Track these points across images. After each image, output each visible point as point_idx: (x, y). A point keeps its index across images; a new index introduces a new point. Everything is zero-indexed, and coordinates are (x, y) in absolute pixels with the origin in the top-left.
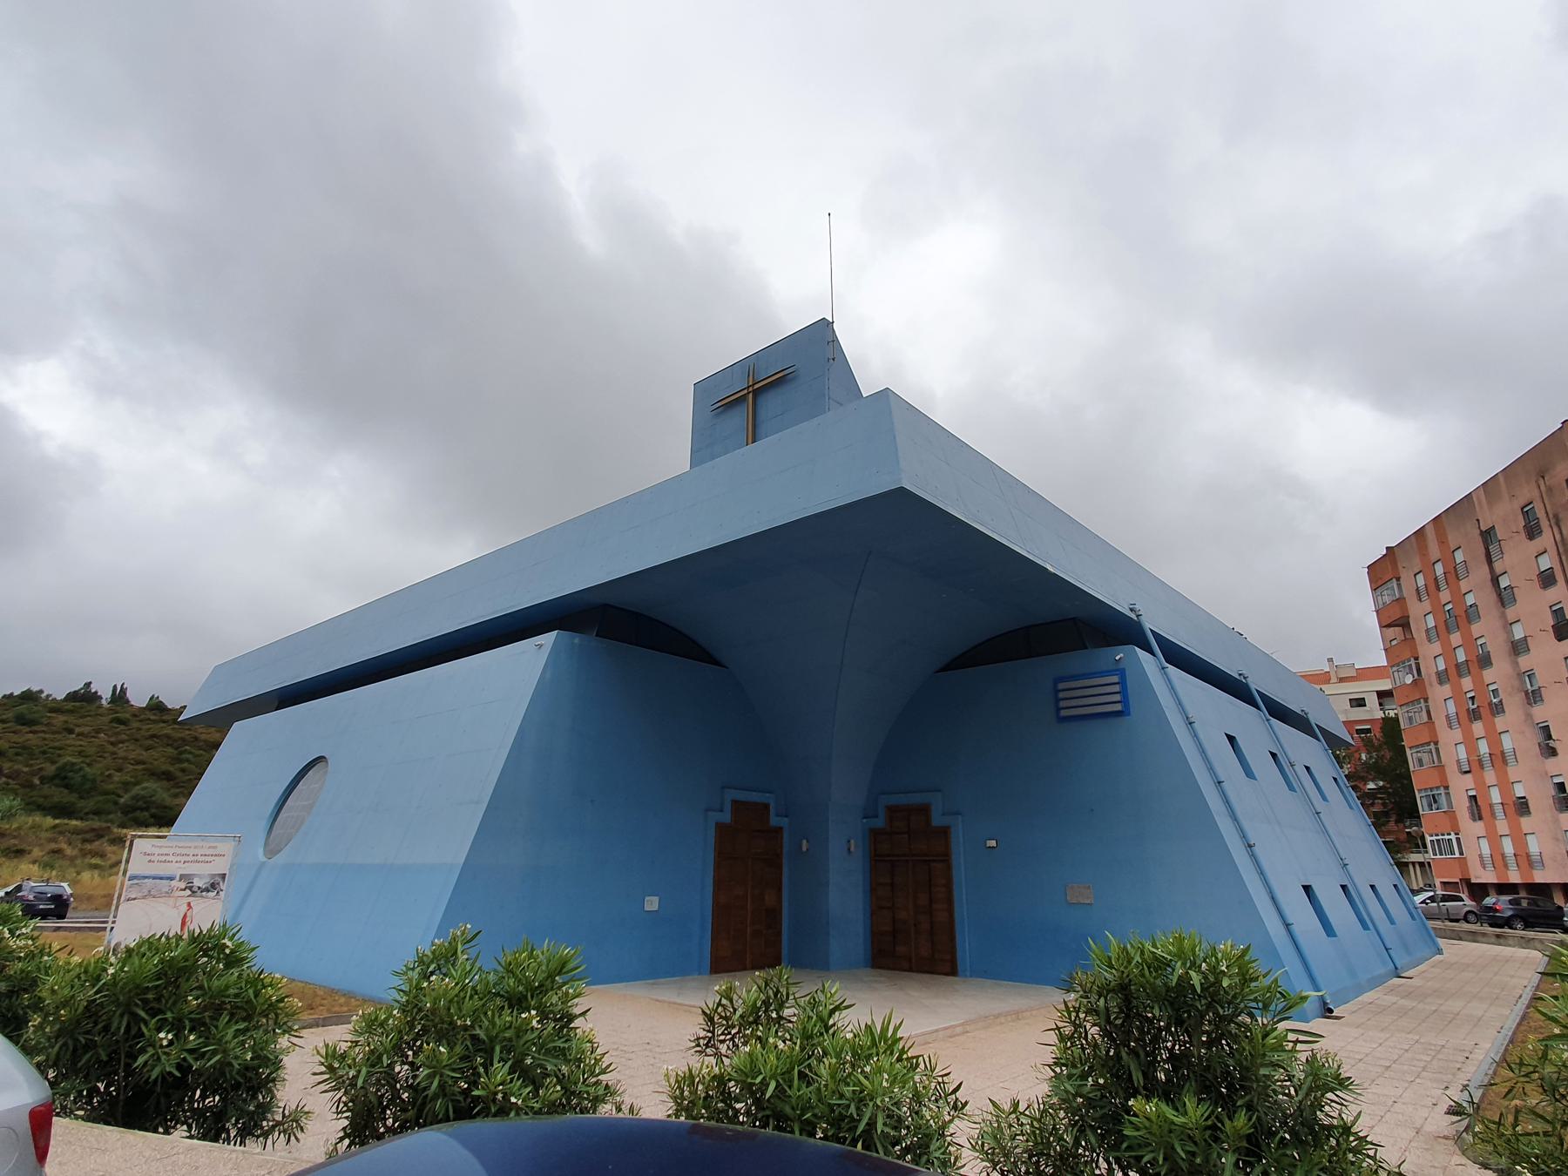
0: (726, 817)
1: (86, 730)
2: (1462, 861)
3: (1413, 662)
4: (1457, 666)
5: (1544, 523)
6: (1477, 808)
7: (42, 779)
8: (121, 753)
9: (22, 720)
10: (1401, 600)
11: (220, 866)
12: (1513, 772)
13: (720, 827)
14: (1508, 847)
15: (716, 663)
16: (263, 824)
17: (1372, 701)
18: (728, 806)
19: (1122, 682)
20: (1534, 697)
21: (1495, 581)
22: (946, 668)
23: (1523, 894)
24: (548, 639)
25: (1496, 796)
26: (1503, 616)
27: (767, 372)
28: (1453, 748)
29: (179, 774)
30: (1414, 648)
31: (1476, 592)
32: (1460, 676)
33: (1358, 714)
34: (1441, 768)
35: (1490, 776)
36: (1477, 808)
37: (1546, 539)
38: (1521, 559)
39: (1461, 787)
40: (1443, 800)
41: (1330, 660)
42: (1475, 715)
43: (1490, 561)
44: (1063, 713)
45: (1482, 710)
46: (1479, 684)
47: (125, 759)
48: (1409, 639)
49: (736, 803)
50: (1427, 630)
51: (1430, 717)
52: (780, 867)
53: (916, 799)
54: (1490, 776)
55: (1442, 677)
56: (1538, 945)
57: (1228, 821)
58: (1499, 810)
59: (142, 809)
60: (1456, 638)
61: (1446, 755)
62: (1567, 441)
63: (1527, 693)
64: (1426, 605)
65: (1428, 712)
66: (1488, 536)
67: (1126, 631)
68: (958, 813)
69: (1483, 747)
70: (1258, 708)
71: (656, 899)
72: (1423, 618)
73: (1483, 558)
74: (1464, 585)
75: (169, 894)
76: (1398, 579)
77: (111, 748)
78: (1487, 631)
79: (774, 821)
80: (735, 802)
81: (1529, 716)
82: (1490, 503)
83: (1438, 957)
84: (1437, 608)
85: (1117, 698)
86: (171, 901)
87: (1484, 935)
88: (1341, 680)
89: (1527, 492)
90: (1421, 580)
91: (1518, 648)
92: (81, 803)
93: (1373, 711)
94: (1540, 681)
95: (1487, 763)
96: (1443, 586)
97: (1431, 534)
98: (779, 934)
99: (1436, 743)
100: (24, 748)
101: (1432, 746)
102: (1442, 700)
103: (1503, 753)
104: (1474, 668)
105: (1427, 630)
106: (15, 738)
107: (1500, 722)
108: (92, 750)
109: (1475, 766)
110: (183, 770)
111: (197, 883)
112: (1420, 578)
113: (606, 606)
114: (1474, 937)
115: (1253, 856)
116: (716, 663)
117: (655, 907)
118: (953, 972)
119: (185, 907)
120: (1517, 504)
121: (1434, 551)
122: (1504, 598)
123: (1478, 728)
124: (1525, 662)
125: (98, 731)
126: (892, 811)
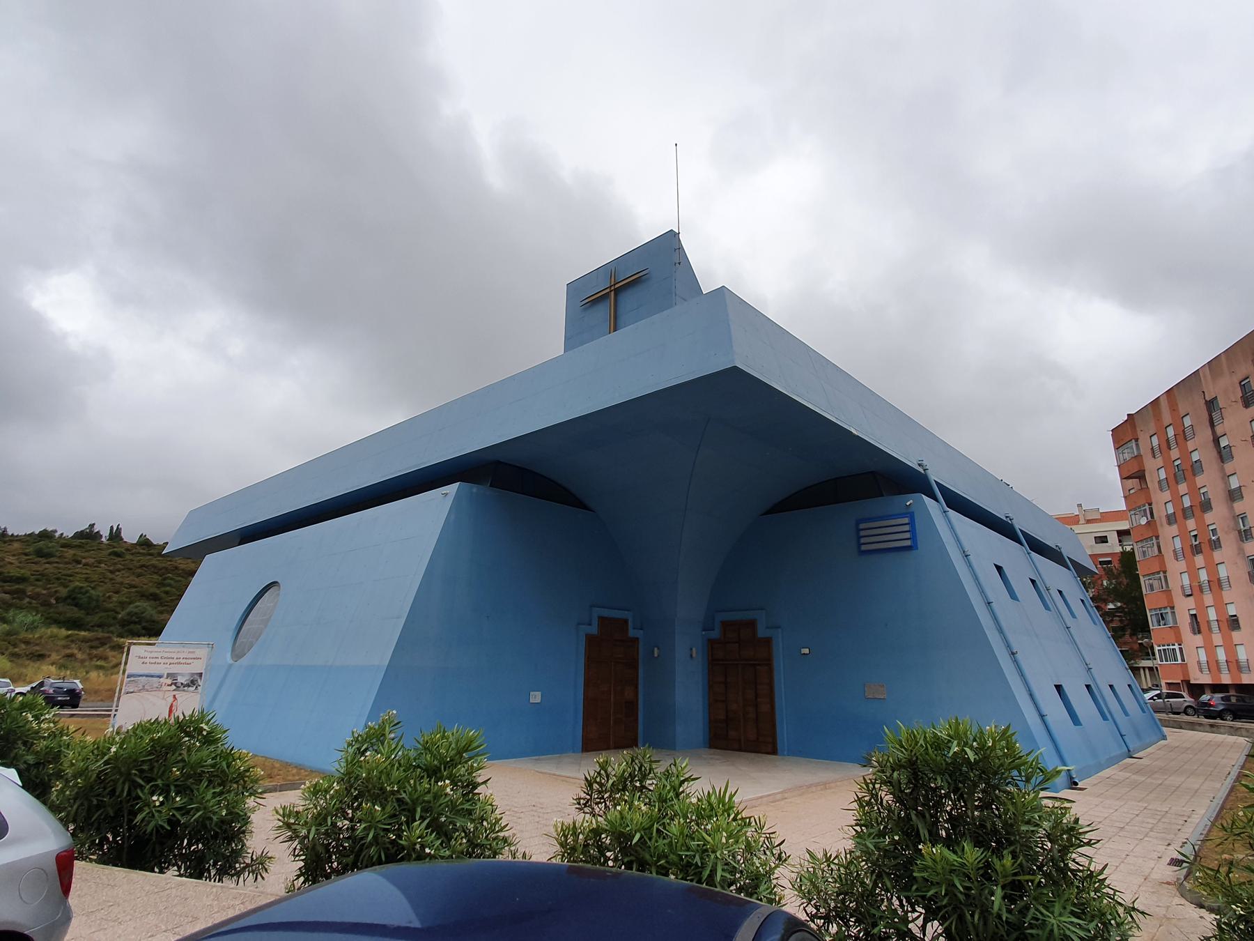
0: (594, 630)
1: (91, 561)
2: (1184, 666)
3: (1147, 507)
4: (1184, 510)
6: (1196, 624)
7: (57, 599)
8: (119, 579)
9: (40, 553)
10: (1138, 457)
11: (198, 667)
12: (1227, 595)
13: (590, 639)
14: (1221, 655)
16: (230, 635)
17: (1113, 538)
18: (595, 622)
19: (912, 523)
20: (1245, 535)
21: (1216, 441)
22: (767, 513)
23: (1232, 692)
24: (453, 489)
25: (1212, 614)
26: (1222, 470)
27: (625, 274)
28: (1178, 576)
29: (163, 595)
31: (1200, 450)
32: (1185, 518)
34: (1168, 592)
35: (1208, 599)
39: (1185, 607)
40: (1169, 617)
41: (1080, 505)
42: (1197, 550)
44: (864, 548)
46: (1201, 525)
47: (122, 583)
48: (1144, 489)
49: (602, 619)
50: (1160, 482)
53: (748, 615)
54: (1208, 599)
55: (1171, 519)
56: (1244, 733)
58: (1215, 626)
59: (135, 623)
60: (1183, 488)
61: (1173, 583)
63: (1240, 532)
64: (1159, 461)
66: (1211, 405)
67: (915, 482)
70: (1021, 543)
71: (538, 694)
72: (1156, 471)
74: (1191, 445)
75: (159, 688)
76: (1137, 440)
78: (1208, 482)
79: (632, 633)
81: (1241, 551)
83: (1163, 742)
84: (1168, 464)
86: (160, 694)
87: (1201, 725)
88: (1089, 522)
89: (1243, 369)
90: (1155, 440)
91: (1234, 495)
92: (89, 618)
93: (1114, 546)
97: (1164, 404)
98: (636, 720)
99: (1165, 572)
100: (43, 575)
101: (1162, 575)
103: (1219, 580)
104: (1197, 511)
106: (35, 567)
107: (1217, 555)
108: (95, 577)
109: (1196, 590)
110: (167, 593)
111: (181, 680)
112: (1155, 439)
114: (1192, 726)
117: (538, 700)
118: (774, 752)
119: (171, 699)
121: (1167, 417)
123: (1199, 560)
124: (1239, 507)
125: (100, 562)
126: (726, 625)
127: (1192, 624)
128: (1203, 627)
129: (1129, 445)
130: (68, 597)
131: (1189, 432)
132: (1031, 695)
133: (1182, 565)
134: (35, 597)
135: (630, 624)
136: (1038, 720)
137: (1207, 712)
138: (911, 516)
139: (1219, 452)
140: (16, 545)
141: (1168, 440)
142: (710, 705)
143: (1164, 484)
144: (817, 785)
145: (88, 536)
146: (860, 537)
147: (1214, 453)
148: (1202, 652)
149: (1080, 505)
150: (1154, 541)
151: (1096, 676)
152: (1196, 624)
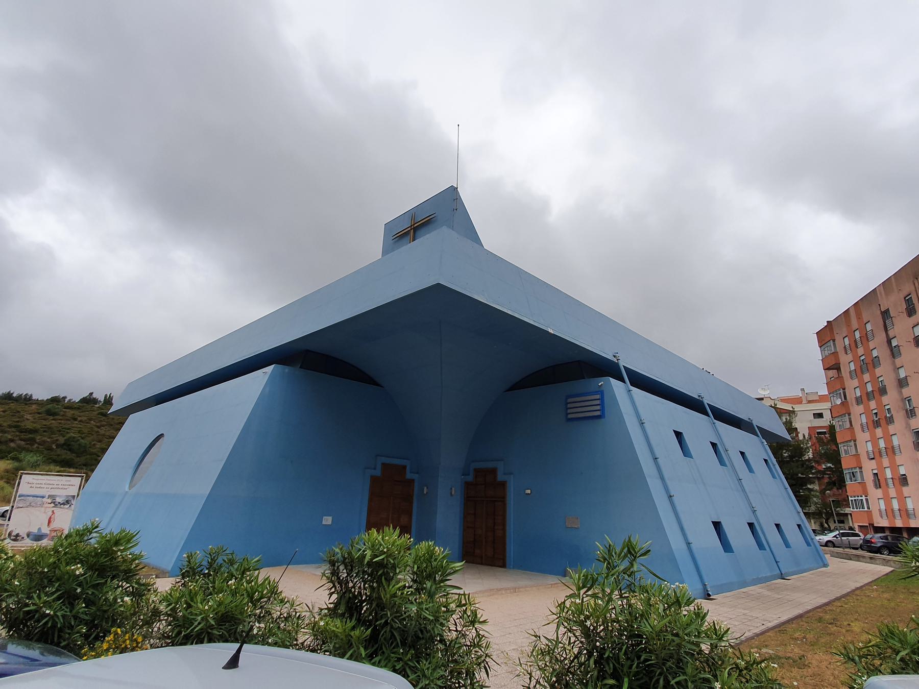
0: (378, 472)
1: (84, 419)
2: (869, 513)
3: (842, 391)
7: (58, 446)
8: (102, 432)
9: (50, 413)
10: (835, 354)
12: (899, 459)
13: (374, 479)
14: (895, 505)
15: (377, 385)
16: (131, 472)
17: (827, 415)
18: (379, 467)
19: (602, 399)
20: (911, 413)
21: (889, 342)
22: (511, 389)
23: (887, 533)
24: (269, 369)
26: (894, 363)
28: (864, 444)
30: (843, 383)
31: (878, 349)
32: (869, 400)
33: (819, 422)
34: (857, 456)
35: (886, 462)
36: (878, 481)
38: (902, 328)
39: (870, 468)
41: (803, 390)
42: (877, 424)
44: (570, 416)
45: (881, 421)
46: (880, 405)
47: (104, 435)
48: (840, 377)
50: (850, 372)
51: (851, 425)
52: (411, 503)
53: (490, 465)
54: (886, 462)
55: (859, 401)
57: (659, 481)
58: (890, 482)
60: (867, 377)
61: (861, 449)
63: (907, 411)
64: (850, 357)
65: (851, 422)
66: (885, 314)
67: (610, 369)
68: (511, 474)
69: (882, 444)
70: (708, 416)
71: (330, 518)
72: (848, 364)
74: (871, 345)
75: (42, 505)
76: (834, 341)
77: (96, 429)
78: (884, 372)
79: (409, 476)
80: (383, 464)
81: (908, 425)
84: (856, 359)
85: (598, 408)
86: (43, 509)
87: (864, 557)
88: (809, 402)
89: (908, 288)
93: (825, 422)
94: (914, 404)
95: (884, 453)
96: (860, 345)
97: (853, 313)
99: (855, 441)
100: (50, 428)
103: (893, 447)
104: (876, 394)
106: (44, 423)
107: (892, 429)
108: (86, 431)
111: (58, 500)
112: (846, 340)
113: (308, 351)
114: (858, 558)
116: (377, 385)
117: (330, 523)
118: (504, 566)
119: (50, 513)
120: (902, 296)
122: (894, 352)
123: (879, 432)
124: (906, 392)
125: (90, 420)
126: (477, 471)
127: (874, 481)
128: (882, 481)
129: (828, 344)
130: (64, 444)
131: (870, 335)
132: (682, 529)
133: (867, 436)
134: (43, 443)
135: (408, 468)
136: (684, 546)
137: (868, 546)
138: (602, 393)
139: (892, 350)
140: (34, 406)
141: (855, 341)
142: (464, 530)
144: (506, 589)
145: (89, 401)
148: (882, 502)
149: (803, 390)
152: (878, 481)
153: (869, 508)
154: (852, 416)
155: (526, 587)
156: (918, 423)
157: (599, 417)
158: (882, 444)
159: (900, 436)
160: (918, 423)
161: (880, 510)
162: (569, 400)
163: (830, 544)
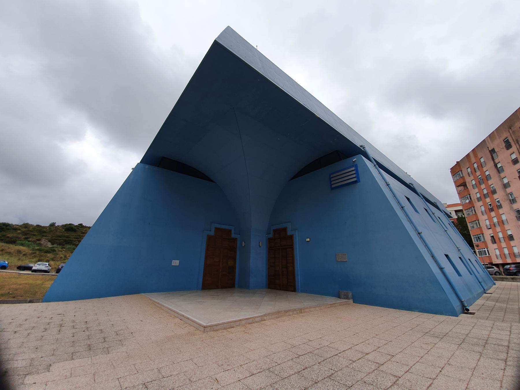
0: (212, 233)
2: (490, 257)
3: (468, 196)
4: (484, 195)
5: (512, 144)
6: (494, 240)
10: (463, 178)
12: (506, 227)
13: (209, 238)
14: (506, 251)
19: (356, 170)
20: (513, 201)
21: (496, 165)
25: (501, 235)
28: (484, 221)
30: (468, 191)
31: (489, 170)
32: (485, 198)
34: (480, 228)
35: (498, 229)
37: (514, 148)
38: (504, 157)
39: (488, 234)
42: (492, 210)
43: (493, 159)
46: (493, 200)
49: (217, 229)
50: (473, 185)
54: (498, 229)
55: (479, 199)
58: (502, 240)
60: (483, 186)
62: (519, 116)
63: (510, 200)
64: (472, 177)
65: (475, 211)
69: (495, 220)
72: (471, 182)
73: (491, 159)
74: (485, 169)
76: (461, 171)
79: (233, 236)
81: (512, 208)
82: (492, 141)
83: (494, 286)
87: (506, 278)
89: (505, 135)
90: (469, 170)
91: (506, 186)
94: (515, 195)
96: (477, 170)
97: (472, 156)
98: (235, 276)
99: (478, 220)
101: (477, 221)
102: (480, 207)
103: (502, 221)
105: (473, 185)
107: (501, 211)
109: (493, 226)
114: (502, 279)
115: (421, 238)
122: (499, 170)
123: (493, 214)
124: (509, 190)
126: (275, 231)
128: (497, 240)
131: (483, 165)
135: (233, 232)
136: (439, 271)
137: (508, 273)
138: (356, 166)
141: (474, 169)
143: (475, 186)
144: (293, 311)
146: (331, 182)
147: (496, 171)
150: (473, 209)
151: (462, 253)
152: (494, 240)
153: (489, 254)
154: (475, 208)
155: (310, 307)
156: (519, 205)
157: (355, 182)
158: (495, 220)
159: (507, 213)
160: (516, 206)
161: (496, 255)
162: (332, 176)
163: (497, 273)
